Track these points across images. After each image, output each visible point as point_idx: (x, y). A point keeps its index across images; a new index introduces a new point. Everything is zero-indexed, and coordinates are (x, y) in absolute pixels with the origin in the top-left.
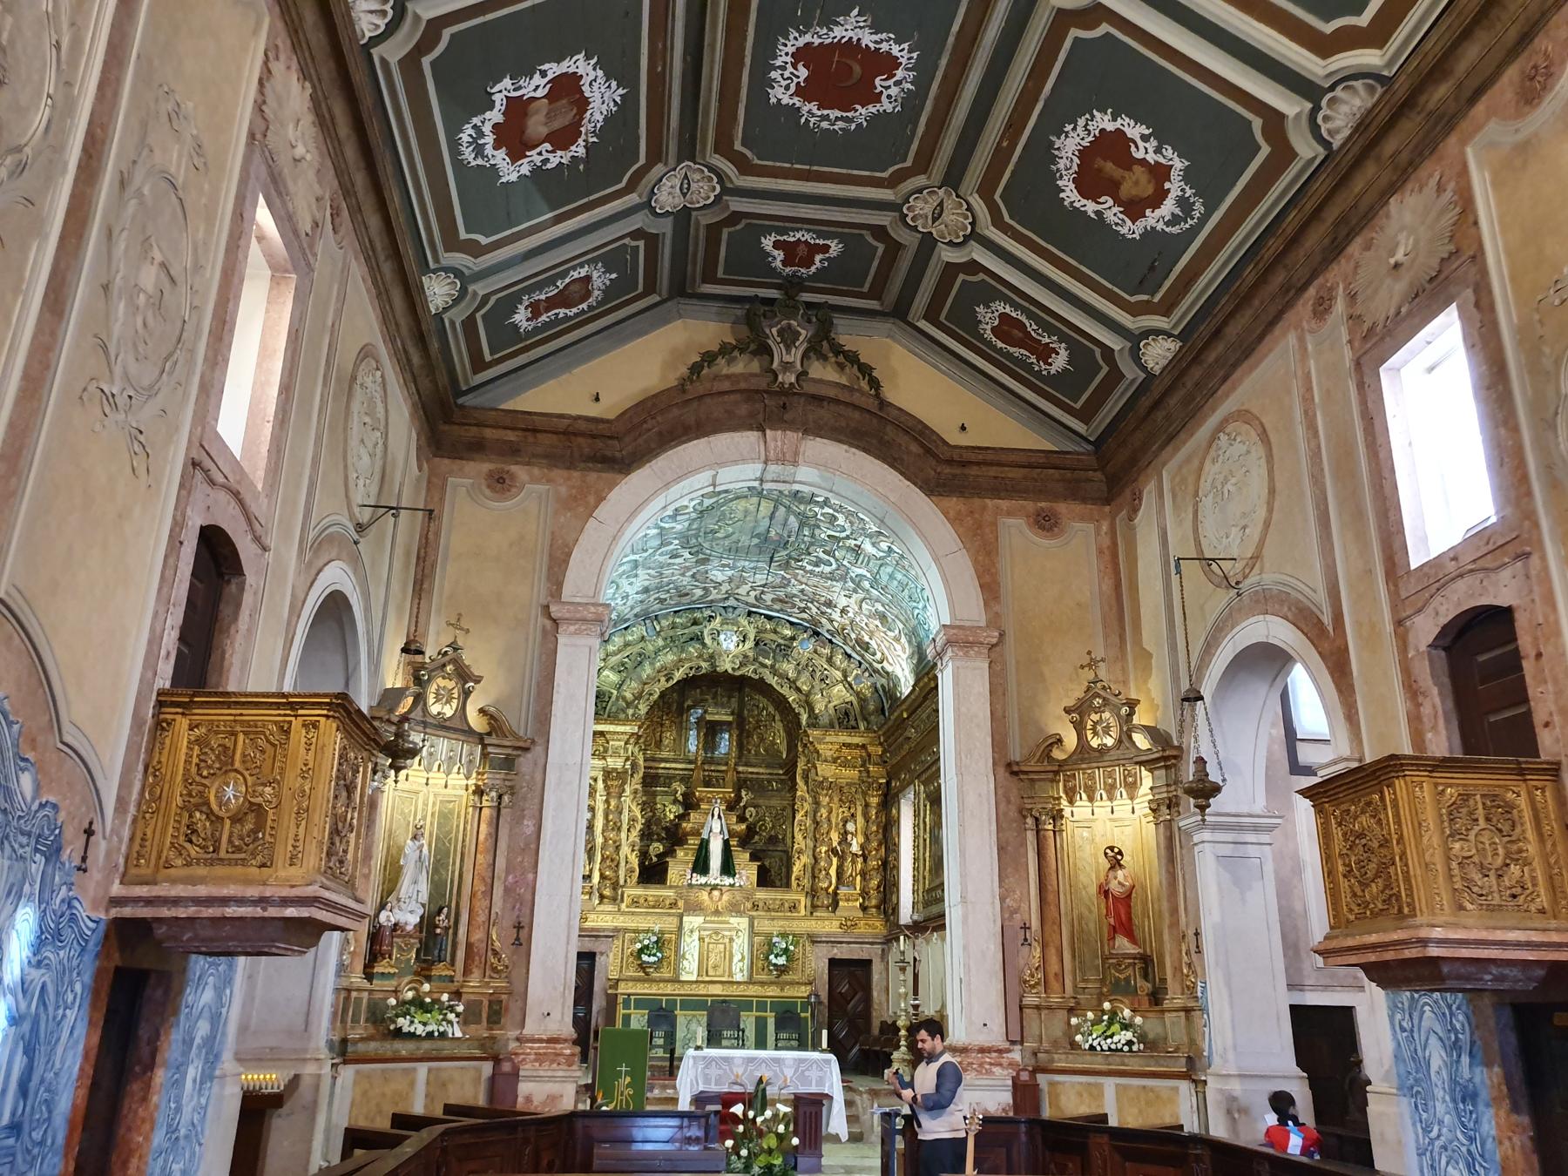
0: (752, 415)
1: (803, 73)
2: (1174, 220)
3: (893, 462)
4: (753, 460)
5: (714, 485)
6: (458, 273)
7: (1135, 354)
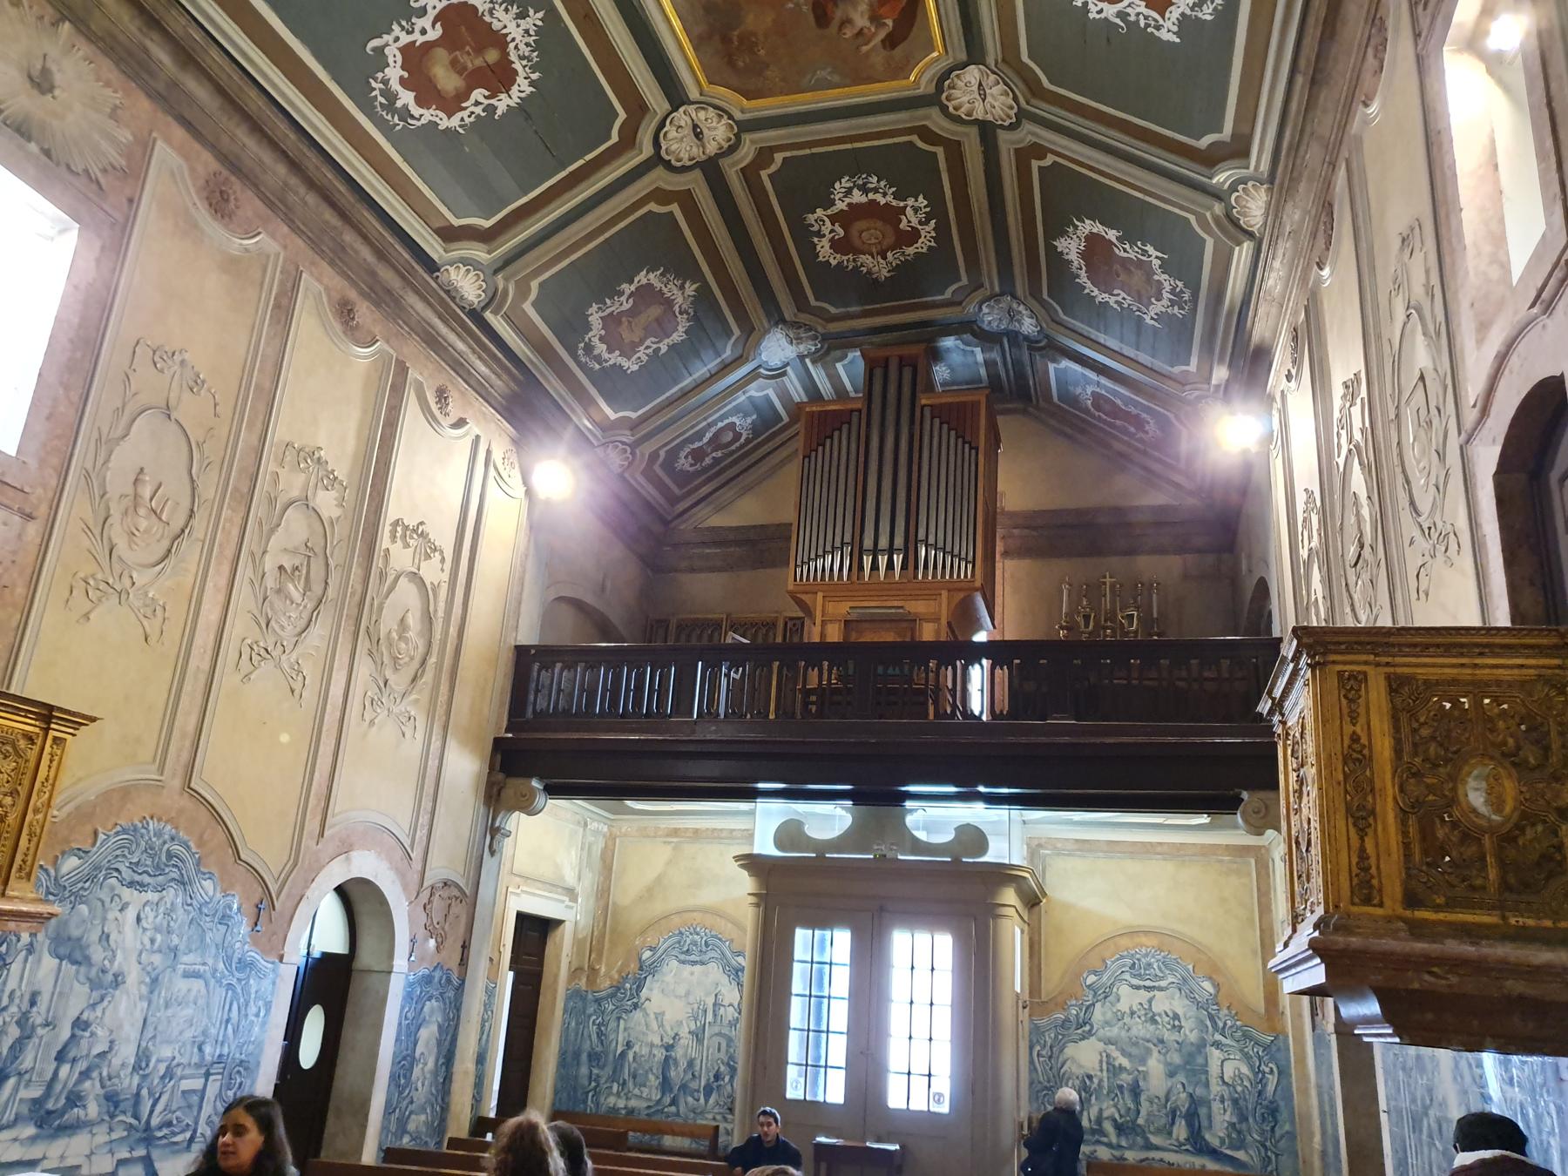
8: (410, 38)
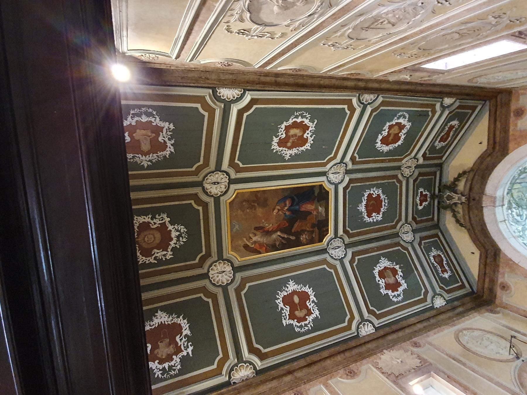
0: (477, 209)
1: (374, 214)
2: (405, 117)
3: (494, 166)
4: (494, 210)
5: (505, 221)
6: (434, 297)
7: (448, 107)
8: (309, 130)
